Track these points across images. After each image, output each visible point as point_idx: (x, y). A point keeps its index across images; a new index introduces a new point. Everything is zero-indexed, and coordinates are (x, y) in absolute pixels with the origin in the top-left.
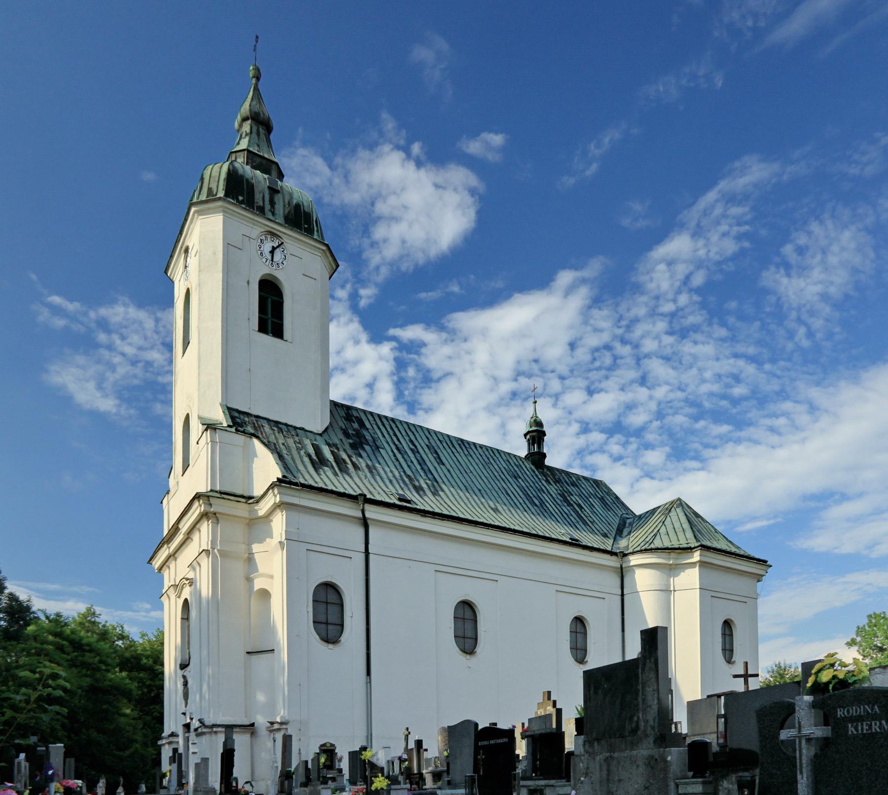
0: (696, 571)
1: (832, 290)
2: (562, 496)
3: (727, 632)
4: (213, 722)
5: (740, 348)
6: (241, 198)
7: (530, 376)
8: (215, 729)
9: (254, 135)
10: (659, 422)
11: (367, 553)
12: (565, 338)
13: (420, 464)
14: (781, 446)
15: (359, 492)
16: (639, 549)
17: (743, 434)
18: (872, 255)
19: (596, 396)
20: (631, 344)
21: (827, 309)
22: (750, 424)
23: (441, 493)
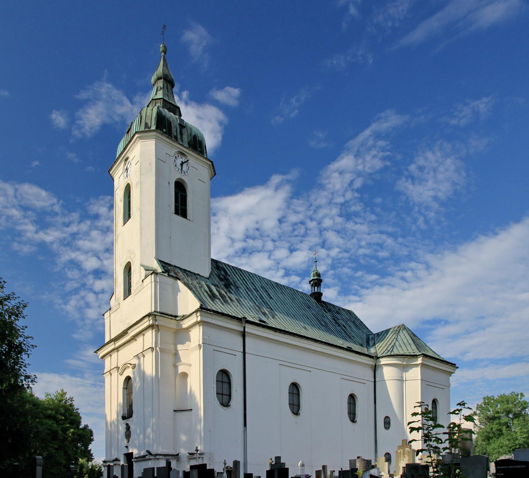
0: (419, 369)
1: (440, 194)
4: (156, 453)
5: (384, 228)
6: (164, 130)
7: (254, 239)
8: (158, 457)
9: (165, 89)
10: (333, 271)
11: (244, 352)
12: (278, 215)
14: (408, 289)
15: (243, 316)
16: (389, 354)
17: (385, 281)
18: (464, 174)
19: (294, 253)
20: (316, 221)
21: (435, 205)
22: (391, 275)
23: (276, 317)
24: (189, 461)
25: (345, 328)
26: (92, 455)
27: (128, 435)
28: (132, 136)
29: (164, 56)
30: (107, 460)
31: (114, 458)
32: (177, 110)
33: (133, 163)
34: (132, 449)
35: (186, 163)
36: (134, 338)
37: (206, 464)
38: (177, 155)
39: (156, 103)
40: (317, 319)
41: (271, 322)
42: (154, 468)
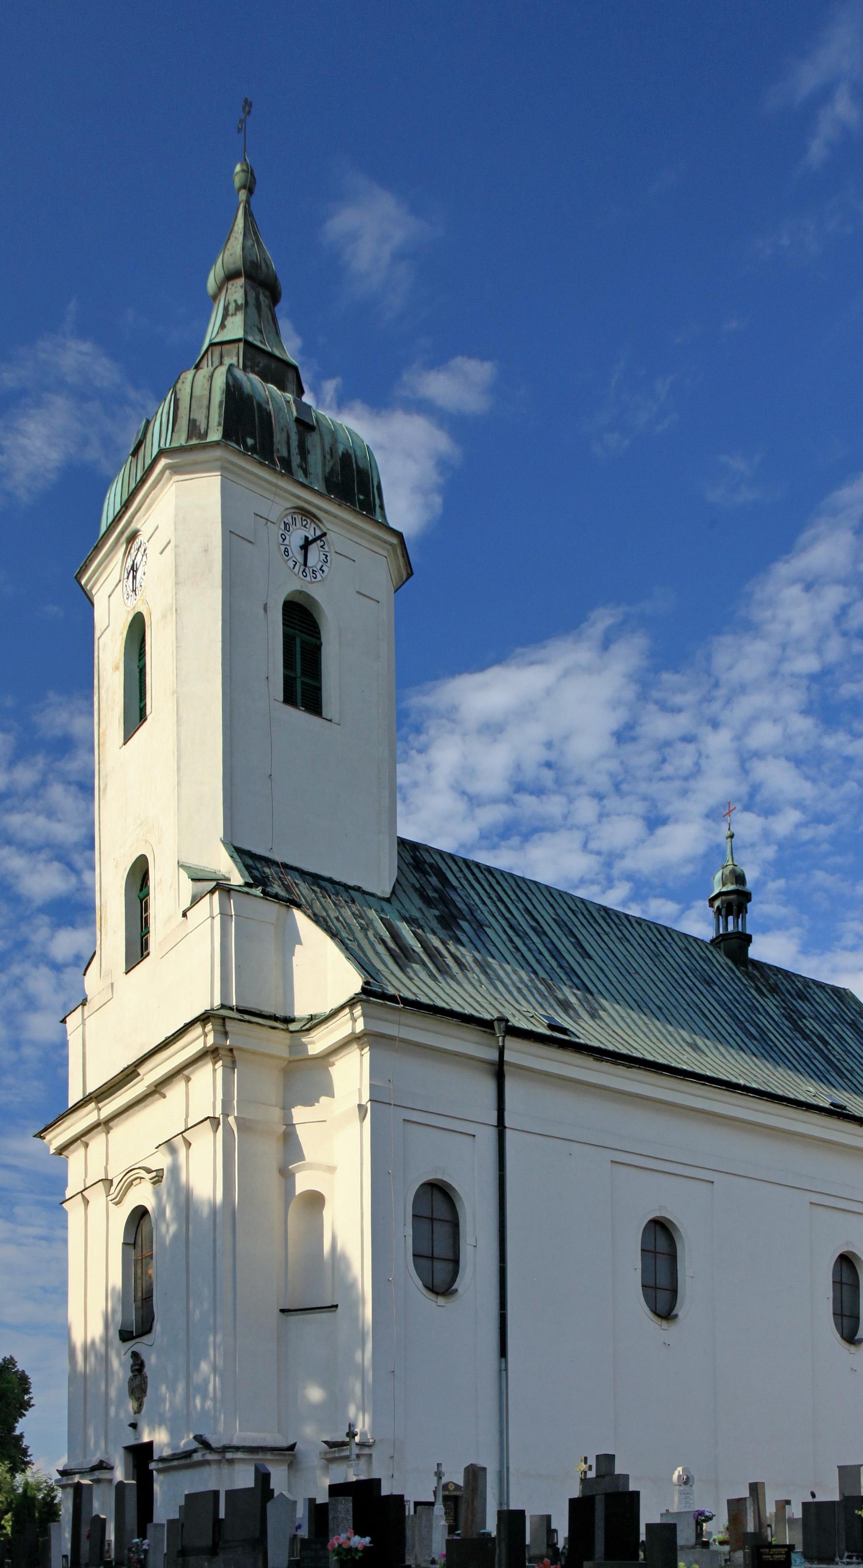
2: (789, 1018)
4: (225, 1442)
6: (250, 441)
7: (539, 791)
8: (229, 1456)
9: (252, 310)
11: (501, 1125)
12: (613, 720)
13: (553, 957)
19: (662, 831)
23: (602, 1013)
24: (326, 1469)
25: (825, 1043)
26: (24, 1452)
27: (138, 1385)
28: (148, 462)
29: (248, 202)
30: (72, 1466)
31: (94, 1461)
32: (291, 375)
33: (153, 548)
34: (152, 1431)
35: (319, 543)
36: (158, 1089)
37: (379, 1480)
38: (289, 520)
39: (222, 357)
40: (734, 1017)
41: (587, 1032)
42: (216, 1493)
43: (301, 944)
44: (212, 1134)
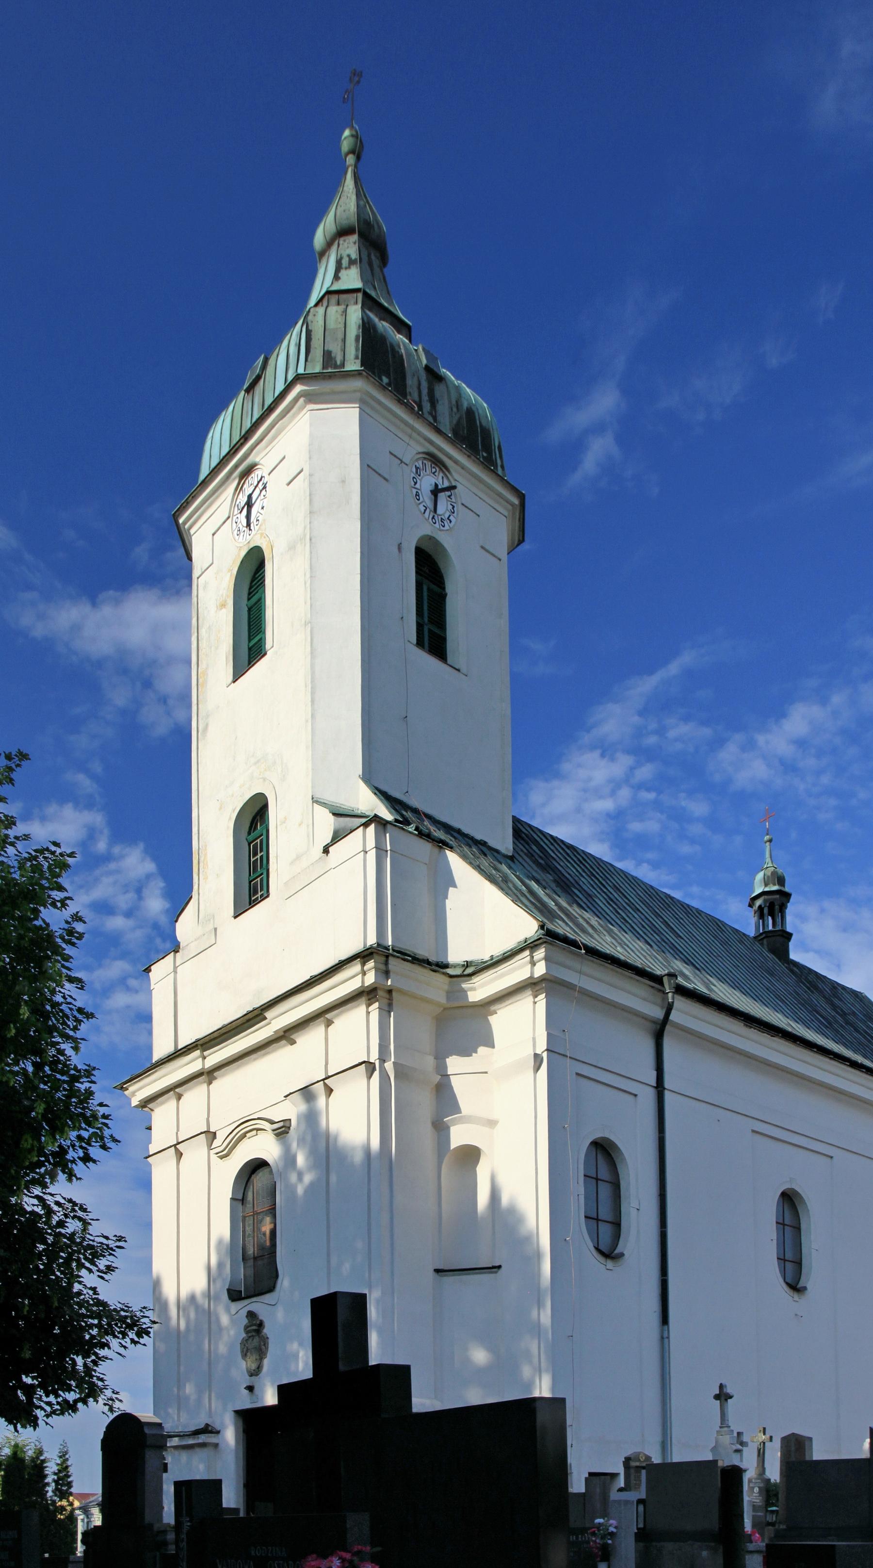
3: (604, 1172)
11: (659, 1087)
33: (276, 483)
35: (448, 493)
36: (287, 1035)
38: (419, 464)
43: (455, 886)
44: (365, 1080)
